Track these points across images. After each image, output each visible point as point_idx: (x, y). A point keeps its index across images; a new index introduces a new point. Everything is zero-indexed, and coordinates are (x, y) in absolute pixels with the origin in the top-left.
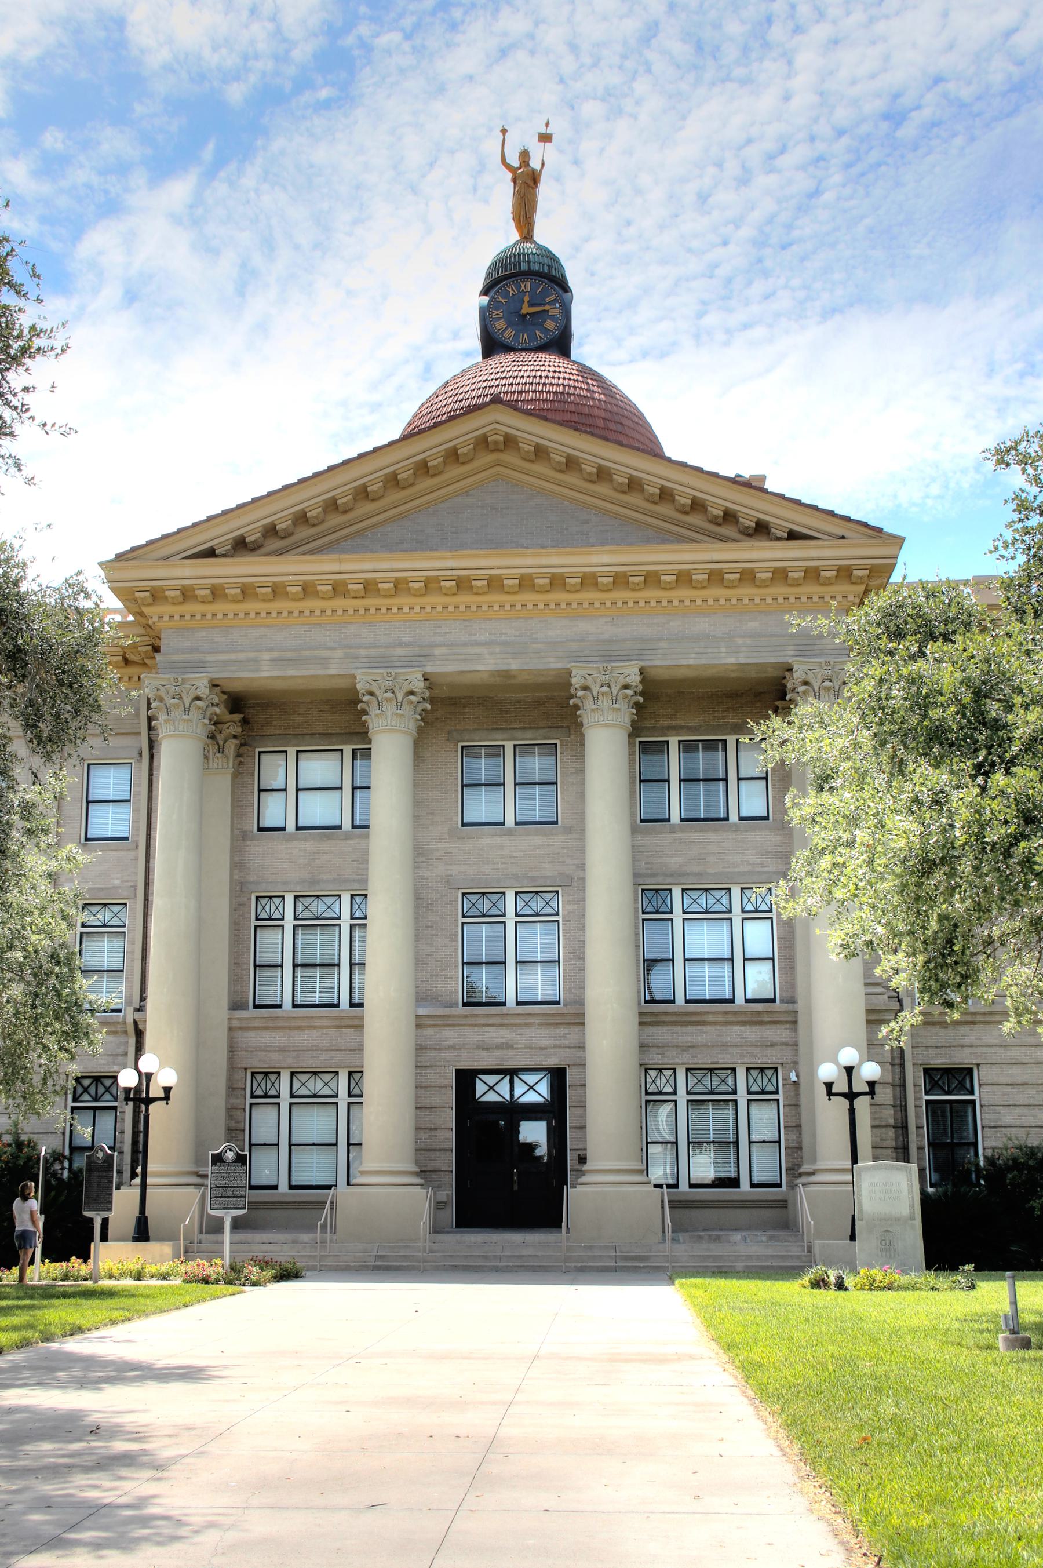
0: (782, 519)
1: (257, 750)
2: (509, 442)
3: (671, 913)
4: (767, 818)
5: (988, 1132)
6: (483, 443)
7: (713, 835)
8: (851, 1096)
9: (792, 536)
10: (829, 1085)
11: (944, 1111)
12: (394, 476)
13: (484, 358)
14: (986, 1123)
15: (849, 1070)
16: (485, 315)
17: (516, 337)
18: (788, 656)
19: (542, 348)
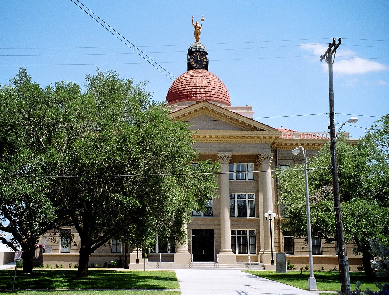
0: (259, 127)
1: (254, 194)
2: (207, 109)
3: (234, 198)
4: (253, 180)
5: (296, 244)
6: (202, 108)
7: (243, 183)
8: (270, 219)
9: (261, 130)
10: (266, 217)
11: (287, 239)
12: (184, 114)
13: (188, 71)
14: (295, 242)
15: (270, 215)
16: (189, 60)
17: (196, 66)
18: (260, 152)
19: (202, 68)
